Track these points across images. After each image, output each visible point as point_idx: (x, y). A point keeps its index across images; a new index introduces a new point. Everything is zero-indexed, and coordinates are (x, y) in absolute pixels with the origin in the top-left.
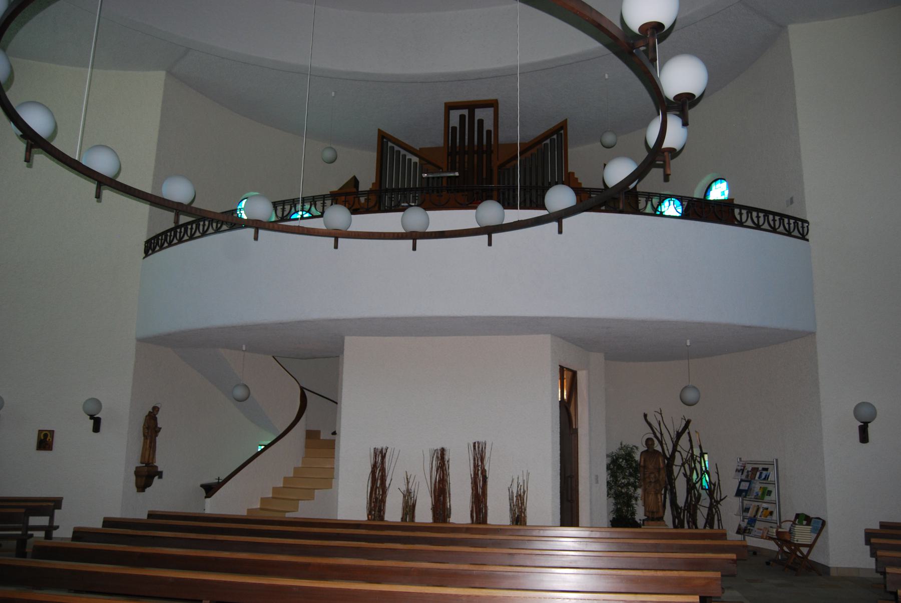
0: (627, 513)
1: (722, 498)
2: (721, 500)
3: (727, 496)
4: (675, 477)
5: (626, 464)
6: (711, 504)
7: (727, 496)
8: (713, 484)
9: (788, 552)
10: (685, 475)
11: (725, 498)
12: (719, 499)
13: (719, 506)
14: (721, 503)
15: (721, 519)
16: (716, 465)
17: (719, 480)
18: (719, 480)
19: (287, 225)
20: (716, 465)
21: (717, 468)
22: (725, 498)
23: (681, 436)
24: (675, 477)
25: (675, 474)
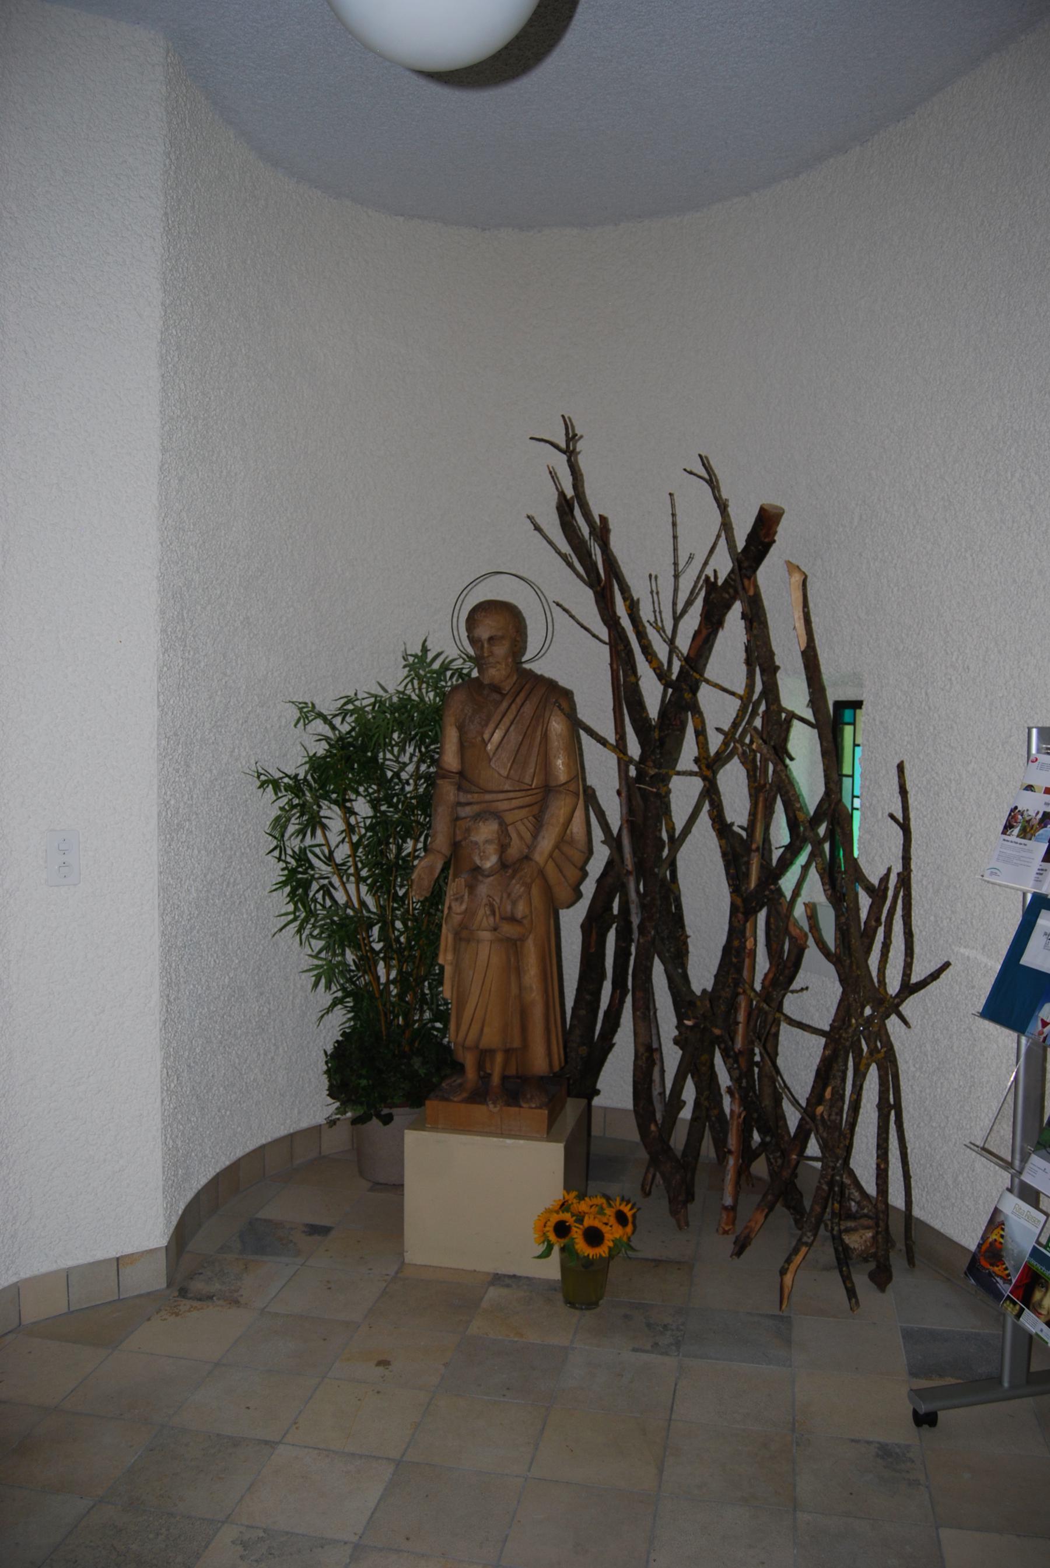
0: (337, 732)
1: (914, 979)
2: (909, 989)
3: (947, 965)
4: (679, 827)
5: (731, 1060)
6: (845, 1010)
7: (947, 965)
8: (870, 889)
9: (766, 702)
10: (722, 827)
11: (935, 976)
12: (893, 986)
13: (893, 1023)
14: (906, 1008)
15: (898, 1107)
16: (901, 768)
17: (906, 859)
18: (906, 859)
19: (579, 990)
20: (901, 768)
21: (903, 792)
22: (935, 976)
23: (909, 825)
24: (679, 827)
25: (679, 816)
